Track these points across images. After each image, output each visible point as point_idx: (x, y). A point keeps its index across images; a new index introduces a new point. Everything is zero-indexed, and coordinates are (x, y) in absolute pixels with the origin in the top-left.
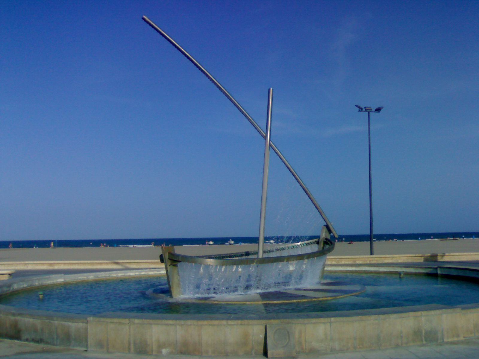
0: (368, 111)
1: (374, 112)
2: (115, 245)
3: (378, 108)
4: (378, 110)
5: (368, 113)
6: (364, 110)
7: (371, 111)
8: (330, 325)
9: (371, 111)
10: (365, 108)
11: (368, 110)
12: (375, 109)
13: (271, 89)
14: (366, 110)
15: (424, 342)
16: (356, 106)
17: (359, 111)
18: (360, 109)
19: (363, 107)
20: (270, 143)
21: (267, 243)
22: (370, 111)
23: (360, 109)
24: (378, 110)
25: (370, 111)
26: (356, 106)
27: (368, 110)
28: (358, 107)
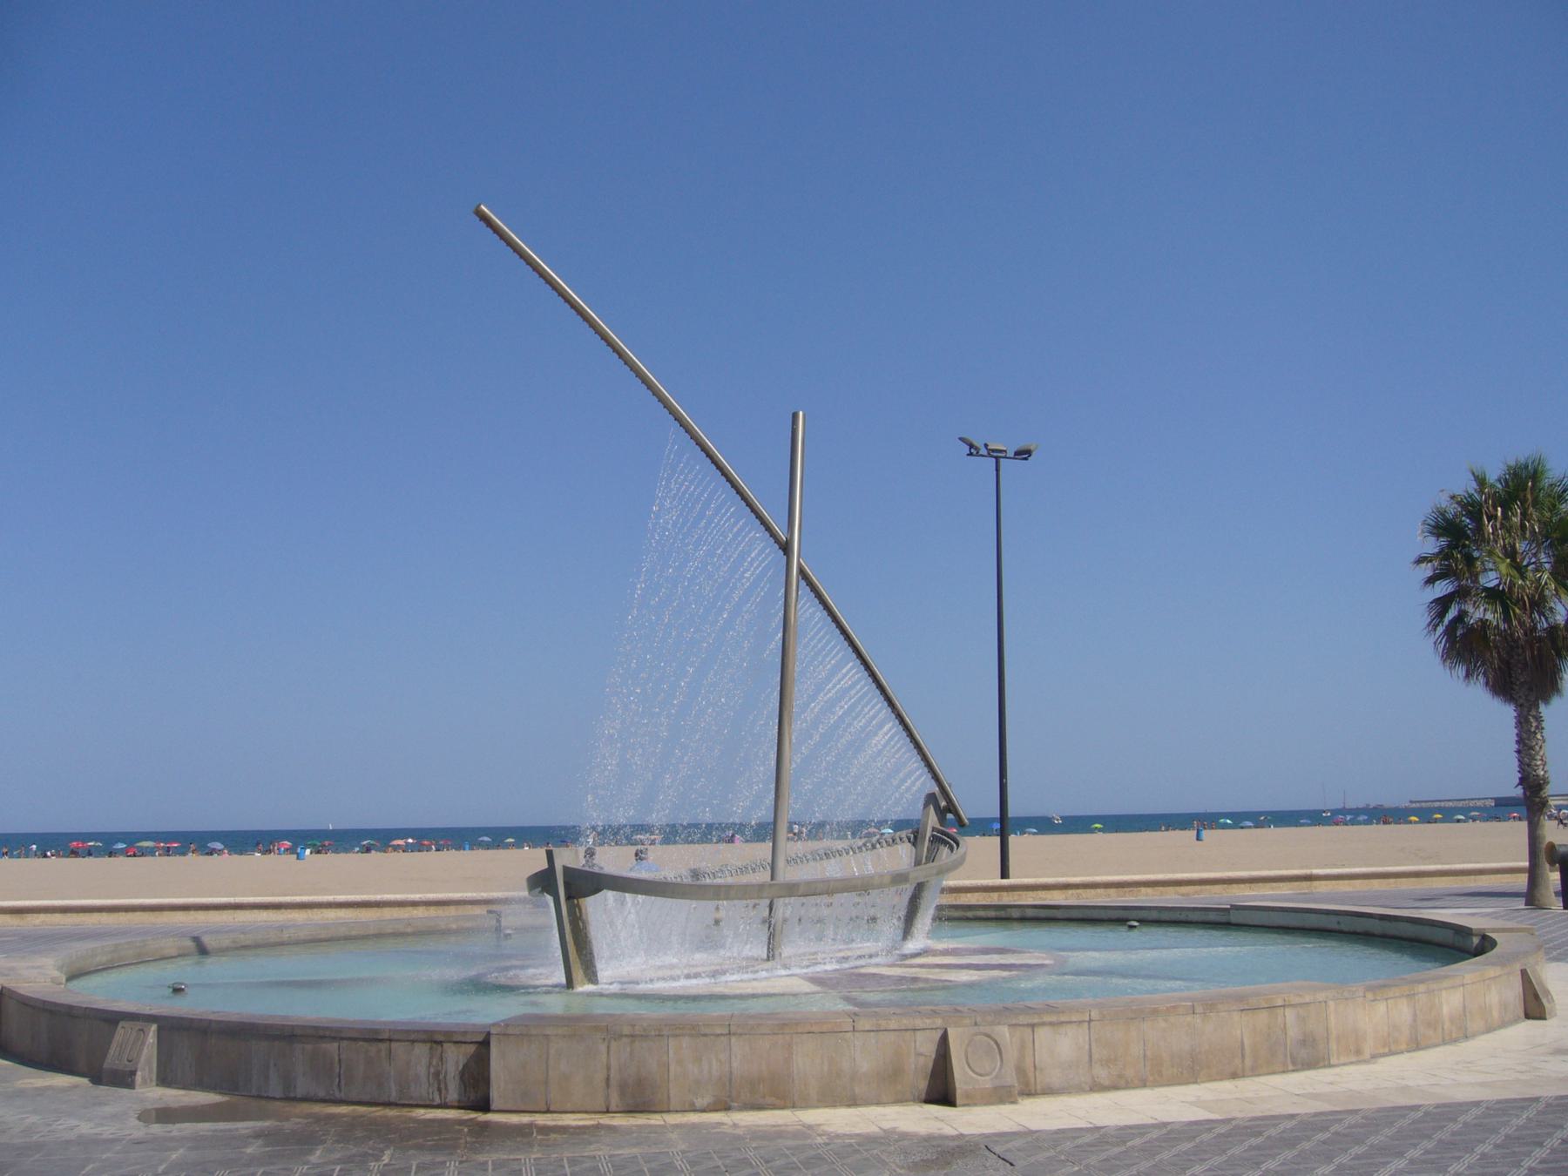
0: (995, 454)
1: (1011, 458)
2: (467, 846)
3: (1026, 448)
4: (1023, 454)
5: (994, 460)
6: (983, 451)
7: (1003, 455)
8: (1089, 1024)
9: (1003, 455)
10: (986, 445)
11: (996, 456)
12: (1016, 449)
13: (801, 413)
14: (989, 450)
15: (1291, 1067)
16: (961, 439)
17: (968, 455)
18: (973, 450)
19: (978, 443)
20: (798, 561)
21: (717, 964)
22: (1000, 455)
23: (973, 450)
24: (1023, 454)
25: (1000, 455)
26: (961, 439)
27: (993, 451)
28: (967, 444)
